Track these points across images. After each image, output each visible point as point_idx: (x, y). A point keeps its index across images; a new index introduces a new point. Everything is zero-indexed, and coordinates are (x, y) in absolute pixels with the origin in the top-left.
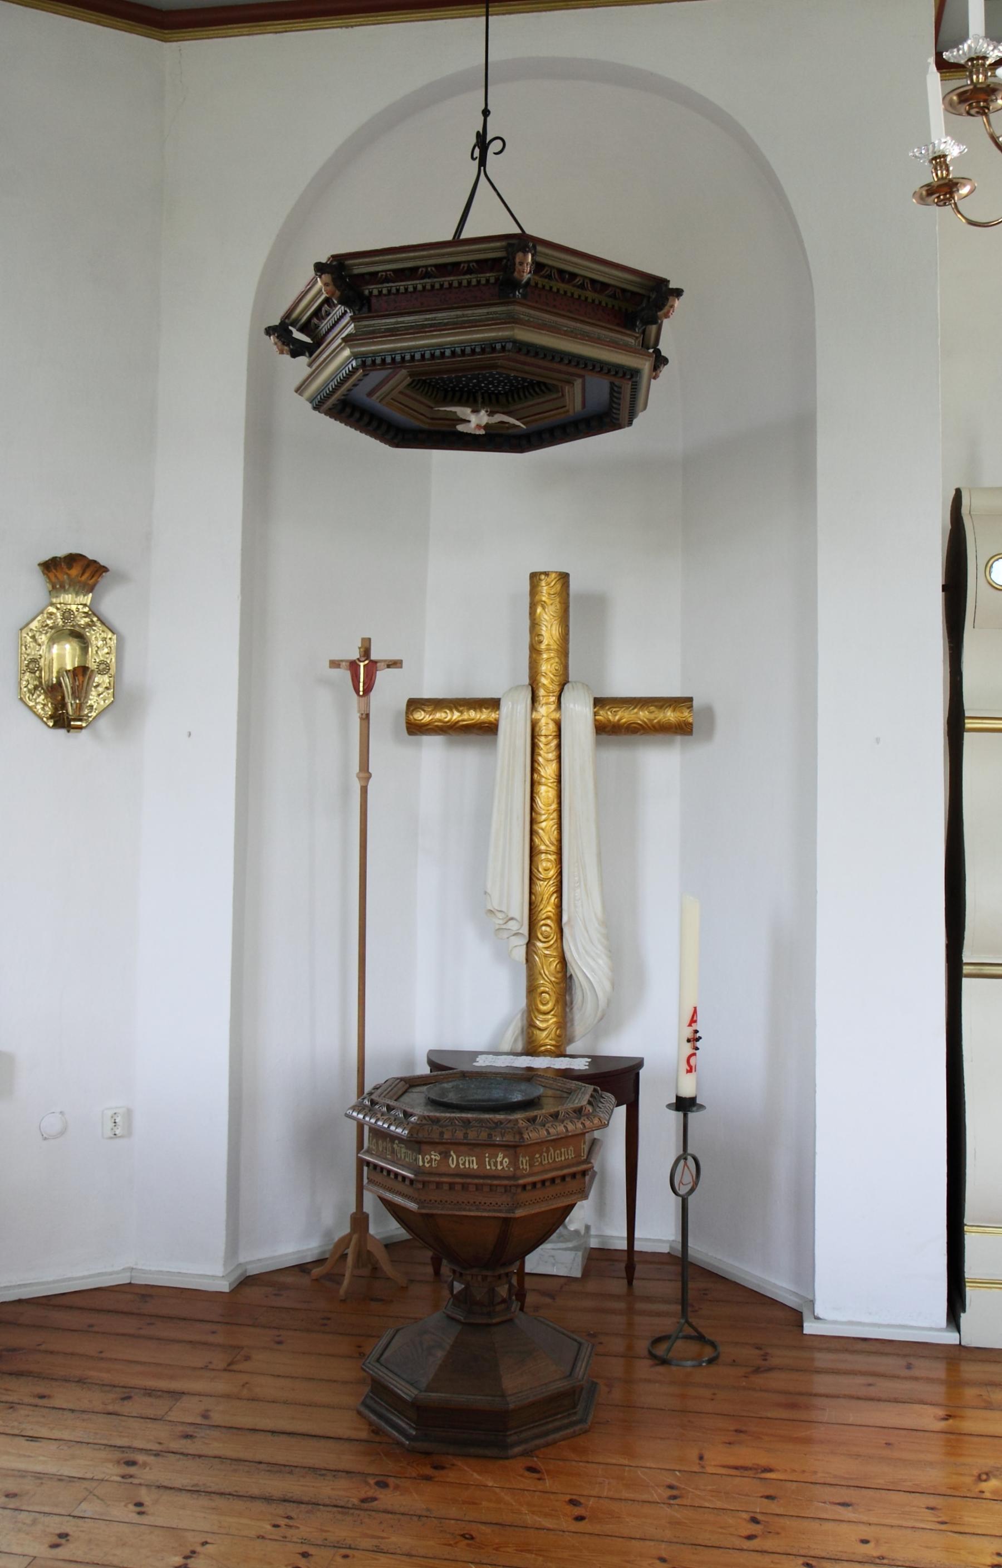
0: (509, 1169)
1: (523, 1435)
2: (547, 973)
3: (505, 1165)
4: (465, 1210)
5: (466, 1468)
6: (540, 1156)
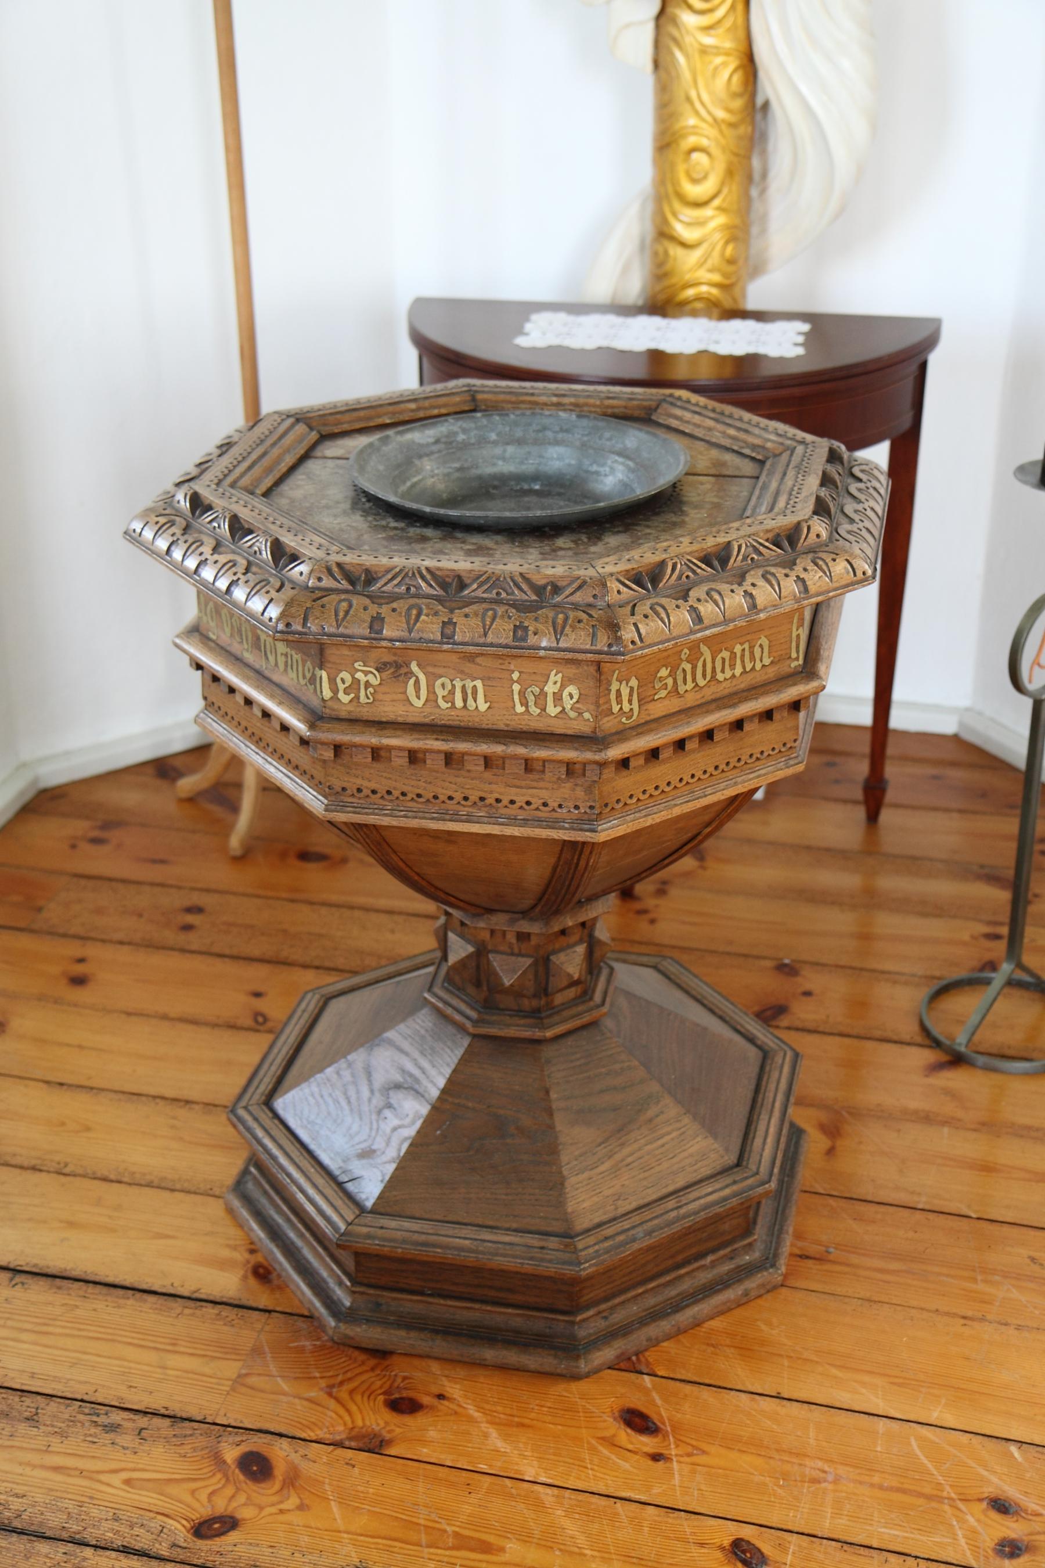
0: (580, 714)
1: (619, 1317)
2: (705, 97)
3: (568, 703)
4: (455, 818)
5: (472, 1411)
6: (672, 674)
